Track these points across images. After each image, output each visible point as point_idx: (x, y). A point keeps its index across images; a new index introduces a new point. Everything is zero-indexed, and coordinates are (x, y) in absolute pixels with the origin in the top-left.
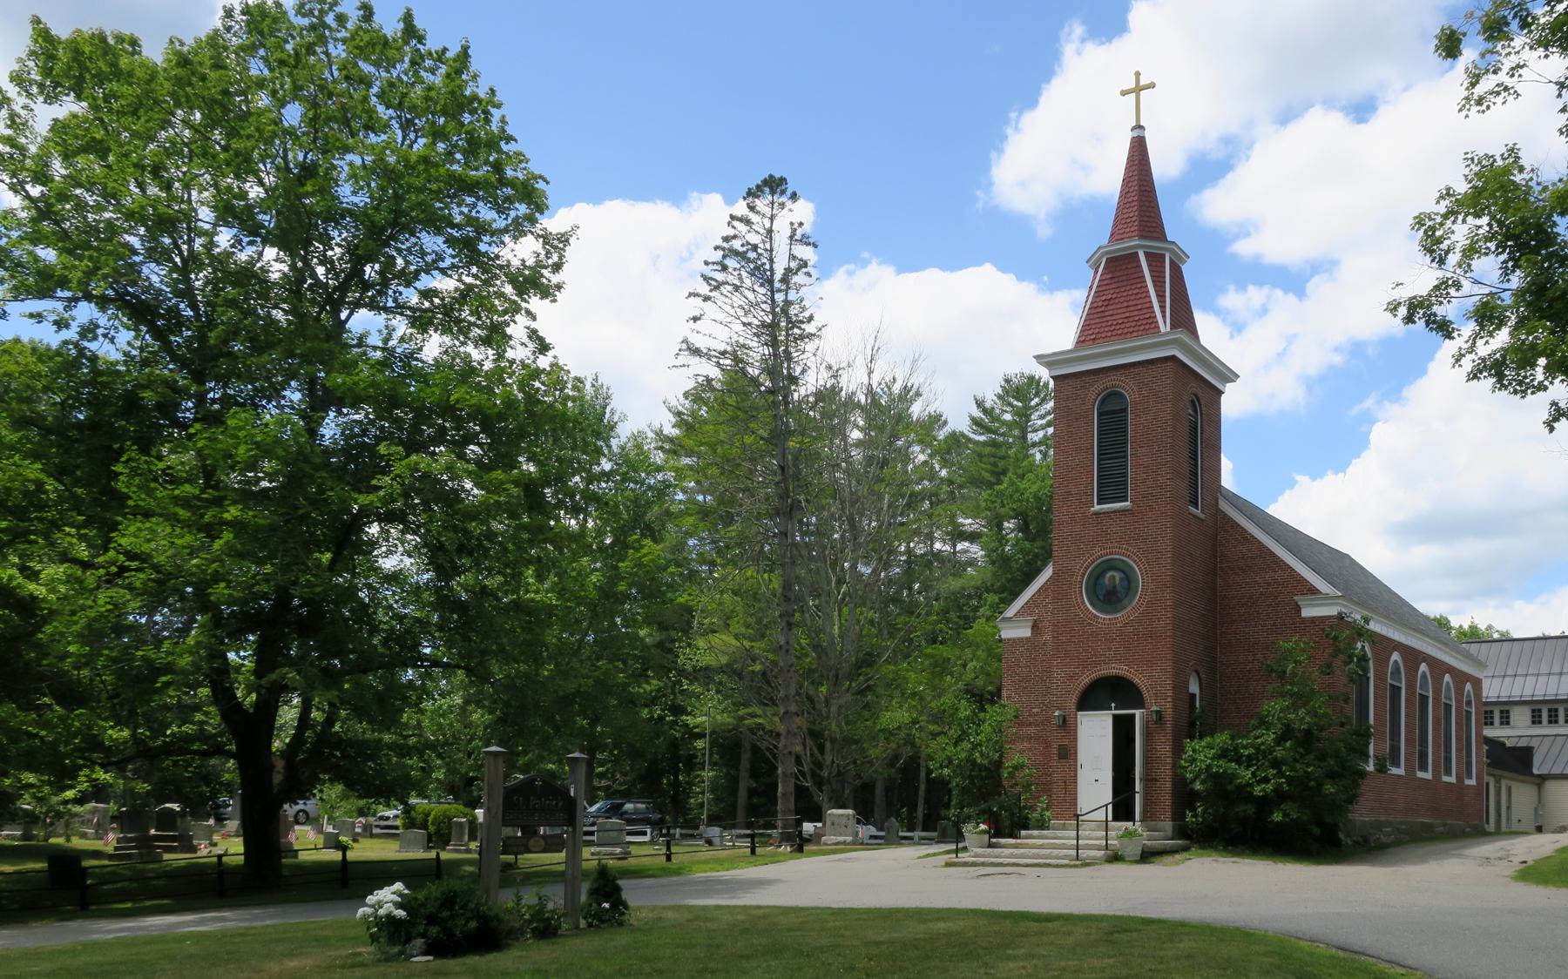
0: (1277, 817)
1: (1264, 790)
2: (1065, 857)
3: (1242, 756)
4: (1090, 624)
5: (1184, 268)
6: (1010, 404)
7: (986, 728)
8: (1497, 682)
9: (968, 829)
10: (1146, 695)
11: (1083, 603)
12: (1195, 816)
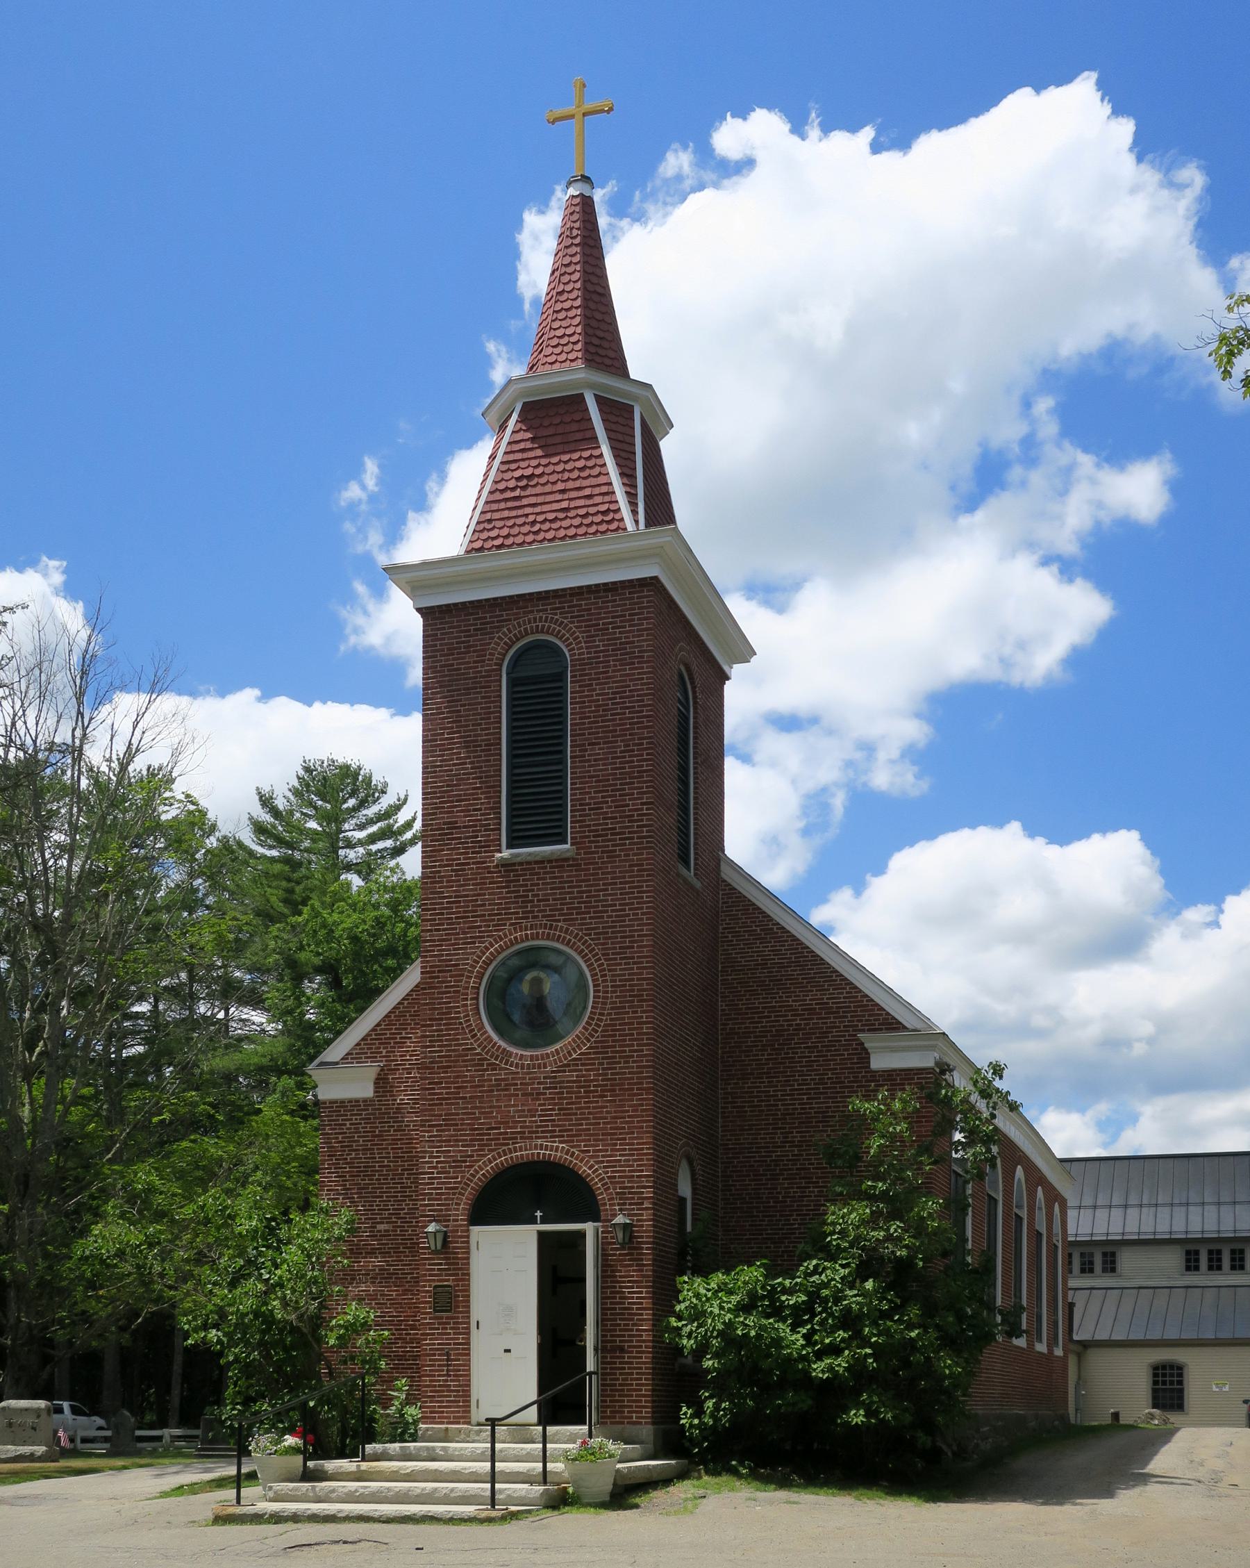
0: (857, 1417)
1: (830, 1368)
2: (465, 1500)
3: (782, 1307)
4: (493, 1067)
5: (663, 444)
6: (311, 804)
7: (292, 1254)
8: (1086, 1215)
9: (261, 1442)
10: (602, 1196)
11: (482, 1027)
12: (699, 1413)
